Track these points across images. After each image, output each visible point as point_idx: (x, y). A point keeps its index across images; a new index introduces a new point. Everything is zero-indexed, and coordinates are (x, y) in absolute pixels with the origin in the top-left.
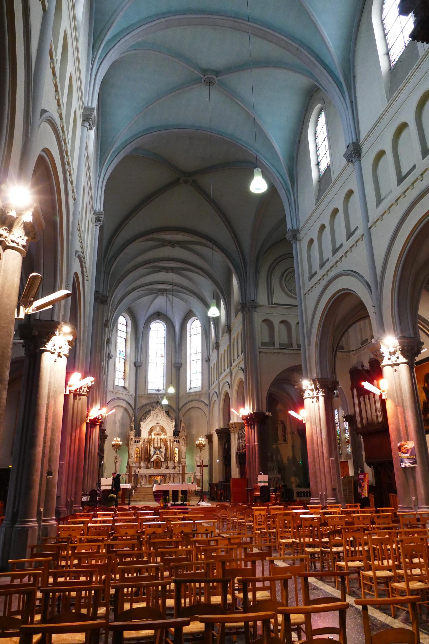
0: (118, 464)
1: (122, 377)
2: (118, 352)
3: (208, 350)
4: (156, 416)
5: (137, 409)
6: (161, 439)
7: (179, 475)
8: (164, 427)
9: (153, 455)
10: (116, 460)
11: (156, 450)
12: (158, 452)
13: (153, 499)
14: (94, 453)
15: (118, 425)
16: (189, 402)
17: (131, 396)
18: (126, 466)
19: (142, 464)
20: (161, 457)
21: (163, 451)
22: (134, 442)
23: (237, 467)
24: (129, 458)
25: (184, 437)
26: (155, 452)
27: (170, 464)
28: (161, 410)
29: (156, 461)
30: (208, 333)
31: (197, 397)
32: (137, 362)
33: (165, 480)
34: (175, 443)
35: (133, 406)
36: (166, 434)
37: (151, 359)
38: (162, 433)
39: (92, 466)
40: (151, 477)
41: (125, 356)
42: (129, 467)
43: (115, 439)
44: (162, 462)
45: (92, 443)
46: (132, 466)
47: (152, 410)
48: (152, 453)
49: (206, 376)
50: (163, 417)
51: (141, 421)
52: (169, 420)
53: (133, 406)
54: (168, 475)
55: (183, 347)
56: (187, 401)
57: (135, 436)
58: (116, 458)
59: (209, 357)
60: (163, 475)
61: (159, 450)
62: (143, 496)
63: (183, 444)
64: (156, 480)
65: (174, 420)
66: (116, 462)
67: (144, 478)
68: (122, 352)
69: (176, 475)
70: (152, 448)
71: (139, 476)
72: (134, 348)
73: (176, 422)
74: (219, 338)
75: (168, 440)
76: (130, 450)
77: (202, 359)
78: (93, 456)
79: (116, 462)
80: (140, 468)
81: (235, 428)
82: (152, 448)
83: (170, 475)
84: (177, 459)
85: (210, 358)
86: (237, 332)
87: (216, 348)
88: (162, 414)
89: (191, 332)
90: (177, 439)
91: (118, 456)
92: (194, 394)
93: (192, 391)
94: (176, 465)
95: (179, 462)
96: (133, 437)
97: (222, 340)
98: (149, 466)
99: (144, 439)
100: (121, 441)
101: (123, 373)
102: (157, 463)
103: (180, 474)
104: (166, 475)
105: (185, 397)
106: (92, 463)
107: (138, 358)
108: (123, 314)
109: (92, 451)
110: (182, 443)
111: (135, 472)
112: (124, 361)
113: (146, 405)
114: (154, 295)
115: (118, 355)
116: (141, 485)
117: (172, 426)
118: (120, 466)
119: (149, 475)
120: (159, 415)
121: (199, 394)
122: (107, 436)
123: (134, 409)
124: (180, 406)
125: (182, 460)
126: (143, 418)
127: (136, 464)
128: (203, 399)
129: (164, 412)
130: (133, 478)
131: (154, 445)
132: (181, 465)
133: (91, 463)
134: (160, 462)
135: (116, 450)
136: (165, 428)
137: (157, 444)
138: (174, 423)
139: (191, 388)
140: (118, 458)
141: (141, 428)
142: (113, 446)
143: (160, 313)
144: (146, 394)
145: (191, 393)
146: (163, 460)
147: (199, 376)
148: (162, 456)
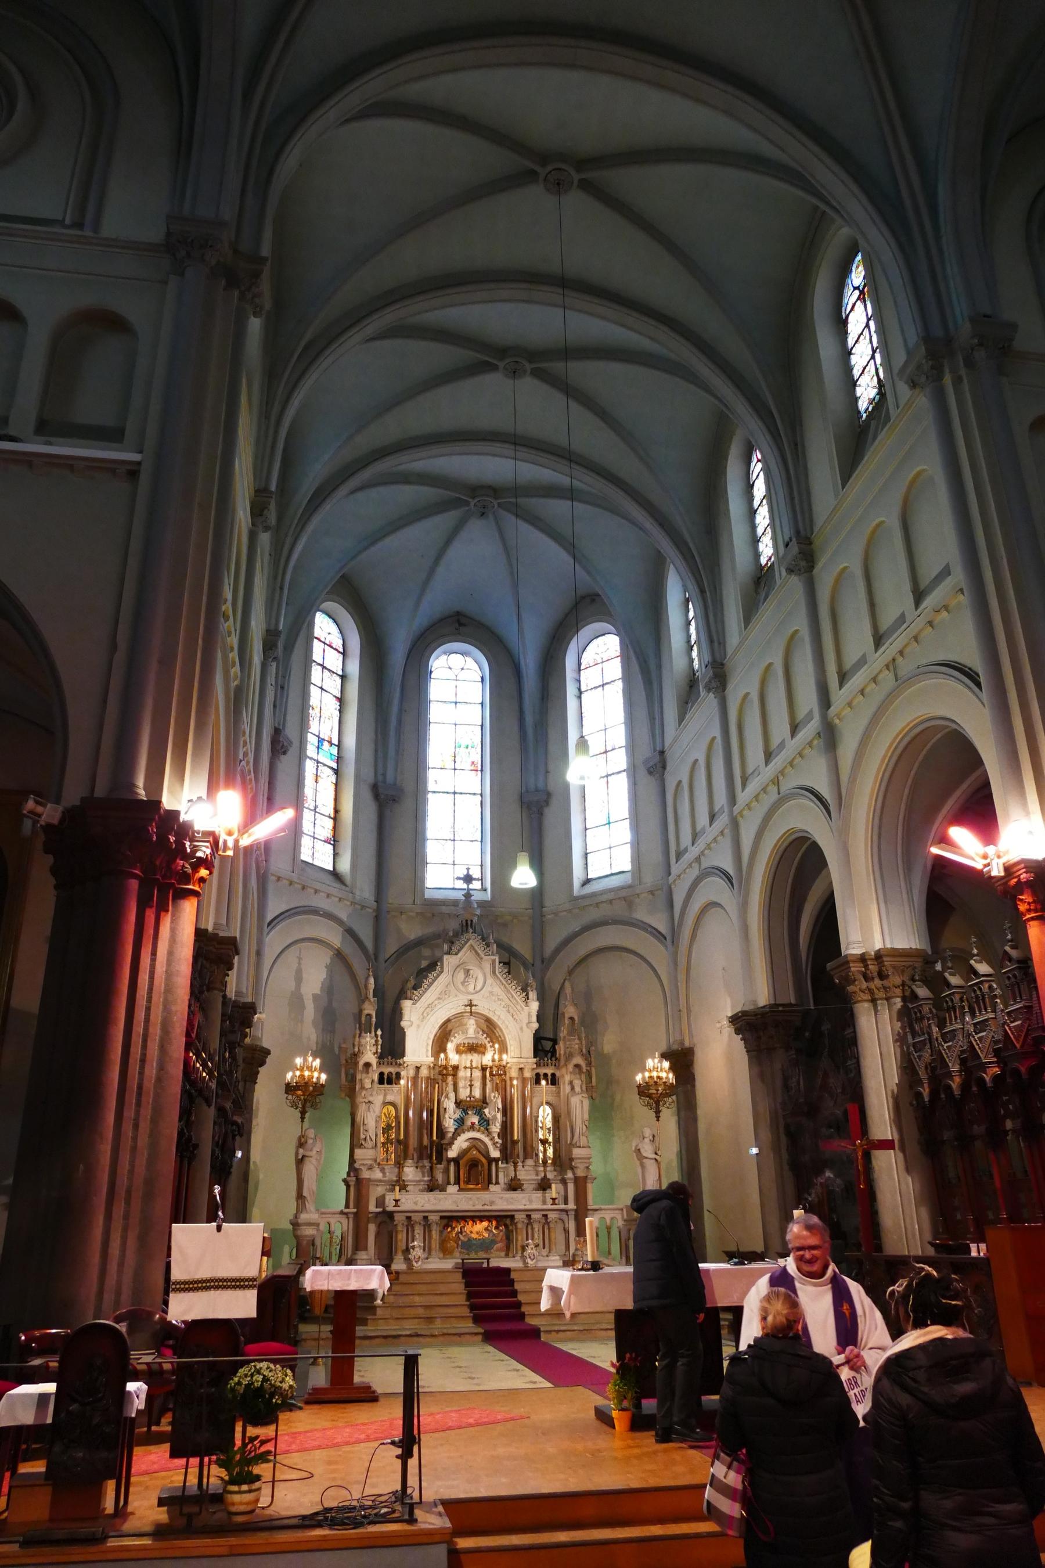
0: (309, 1169)
1: (328, 834)
2: (312, 740)
3: (657, 732)
4: (461, 975)
5: (383, 957)
6: (484, 1069)
7: (564, 1217)
8: (495, 1019)
9: (457, 1133)
10: (301, 1151)
11: (465, 1111)
12: (475, 1119)
13: (469, 1326)
14: (161, 1067)
15: (310, 1011)
16: (586, 929)
17: (363, 907)
18: (344, 1181)
19: (410, 1172)
20: (486, 1140)
21: (495, 1118)
22: (376, 1077)
23: (908, 1170)
24: (355, 1143)
25: (578, 1060)
26: (461, 1122)
27: (527, 1173)
28: (483, 956)
29: (469, 1156)
30: (653, 666)
31: (619, 910)
32: (384, 782)
33: (508, 1239)
34: (543, 1082)
35: (369, 945)
36: (503, 1049)
37: (436, 779)
38: (488, 1045)
39: (143, 1140)
40: (446, 1226)
41: (339, 759)
42: (356, 1184)
43: (299, 1061)
44: (491, 1160)
45: (149, 1000)
46: (369, 1180)
47: (448, 953)
48: (450, 1125)
49: (653, 825)
50: (490, 981)
51: (402, 995)
52: (519, 997)
53: (369, 945)
54: (520, 1217)
55: (553, 735)
56: (576, 927)
57: (381, 1057)
58: (301, 1143)
59: (662, 753)
60: (496, 1218)
61: (480, 1113)
62: (421, 1311)
63: (577, 1089)
64: (470, 1239)
65: (533, 995)
66: (300, 1162)
67: (418, 1231)
68: (326, 744)
69: (552, 1216)
70: (450, 1104)
71: (399, 1218)
72: (372, 735)
73: (541, 999)
74: (722, 643)
75: (514, 1073)
76: (362, 1108)
77: (632, 771)
78: (149, 1084)
79: (300, 1162)
80: (401, 1185)
81: (877, 982)
82: (450, 1104)
83: (529, 1217)
84: (550, 1152)
85: (668, 754)
86: (708, 739)
87: (714, 684)
88: (487, 967)
89: (579, 681)
90: (549, 1071)
91: (311, 1133)
92: (604, 898)
93: (589, 889)
94: (550, 1176)
95: (562, 1162)
96: (373, 1060)
97: (675, 740)
98: (440, 1177)
99: (418, 1068)
100: (322, 1069)
101: (331, 822)
102: (474, 1164)
103: (566, 1211)
104: (512, 1217)
105: (570, 911)
106: (144, 1126)
107: (385, 767)
108: (329, 605)
109: (145, 1046)
110: (571, 1083)
111: (381, 1201)
112: (333, 779)
113: (419, 943)
114: (451, 517)
115: (311, 750)
116: (407, 1260)
117: (529, 1015)
118: (320, 1177)
119: (442, 1218)
120: (476, 972)
121: (625, 899)
122: (267, 1052)
123: (373, 958)
124: (549, 950)
125: (576, 1152)
126: (410, 985)
127: (383, 1171)
128: (641, 914)
129: (494, 961)
130: (372, 1228)
131: (456, 1090)
132: (570, 1175)
133: (136, 1126)
134: (483, 1160)
135: (304, 1107)
136: (499, 1023)
137: (469, 1087)
138: (535, 1006)
139: (587, 881)
140: (310, 1141)
141: (403, 1024)
142: (289, 1088)
143: (465, 616)
144: (418, 902)
145: (594, 895)
146: (495, 1154)
147: (623, 833)
148: (492, 1139)
